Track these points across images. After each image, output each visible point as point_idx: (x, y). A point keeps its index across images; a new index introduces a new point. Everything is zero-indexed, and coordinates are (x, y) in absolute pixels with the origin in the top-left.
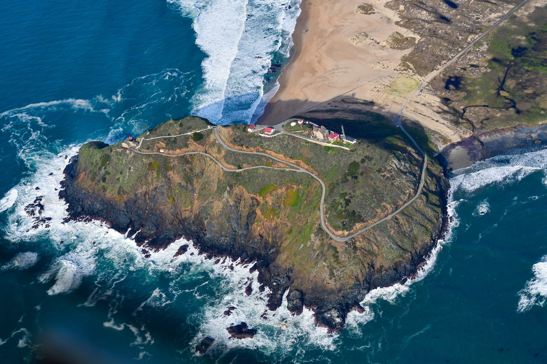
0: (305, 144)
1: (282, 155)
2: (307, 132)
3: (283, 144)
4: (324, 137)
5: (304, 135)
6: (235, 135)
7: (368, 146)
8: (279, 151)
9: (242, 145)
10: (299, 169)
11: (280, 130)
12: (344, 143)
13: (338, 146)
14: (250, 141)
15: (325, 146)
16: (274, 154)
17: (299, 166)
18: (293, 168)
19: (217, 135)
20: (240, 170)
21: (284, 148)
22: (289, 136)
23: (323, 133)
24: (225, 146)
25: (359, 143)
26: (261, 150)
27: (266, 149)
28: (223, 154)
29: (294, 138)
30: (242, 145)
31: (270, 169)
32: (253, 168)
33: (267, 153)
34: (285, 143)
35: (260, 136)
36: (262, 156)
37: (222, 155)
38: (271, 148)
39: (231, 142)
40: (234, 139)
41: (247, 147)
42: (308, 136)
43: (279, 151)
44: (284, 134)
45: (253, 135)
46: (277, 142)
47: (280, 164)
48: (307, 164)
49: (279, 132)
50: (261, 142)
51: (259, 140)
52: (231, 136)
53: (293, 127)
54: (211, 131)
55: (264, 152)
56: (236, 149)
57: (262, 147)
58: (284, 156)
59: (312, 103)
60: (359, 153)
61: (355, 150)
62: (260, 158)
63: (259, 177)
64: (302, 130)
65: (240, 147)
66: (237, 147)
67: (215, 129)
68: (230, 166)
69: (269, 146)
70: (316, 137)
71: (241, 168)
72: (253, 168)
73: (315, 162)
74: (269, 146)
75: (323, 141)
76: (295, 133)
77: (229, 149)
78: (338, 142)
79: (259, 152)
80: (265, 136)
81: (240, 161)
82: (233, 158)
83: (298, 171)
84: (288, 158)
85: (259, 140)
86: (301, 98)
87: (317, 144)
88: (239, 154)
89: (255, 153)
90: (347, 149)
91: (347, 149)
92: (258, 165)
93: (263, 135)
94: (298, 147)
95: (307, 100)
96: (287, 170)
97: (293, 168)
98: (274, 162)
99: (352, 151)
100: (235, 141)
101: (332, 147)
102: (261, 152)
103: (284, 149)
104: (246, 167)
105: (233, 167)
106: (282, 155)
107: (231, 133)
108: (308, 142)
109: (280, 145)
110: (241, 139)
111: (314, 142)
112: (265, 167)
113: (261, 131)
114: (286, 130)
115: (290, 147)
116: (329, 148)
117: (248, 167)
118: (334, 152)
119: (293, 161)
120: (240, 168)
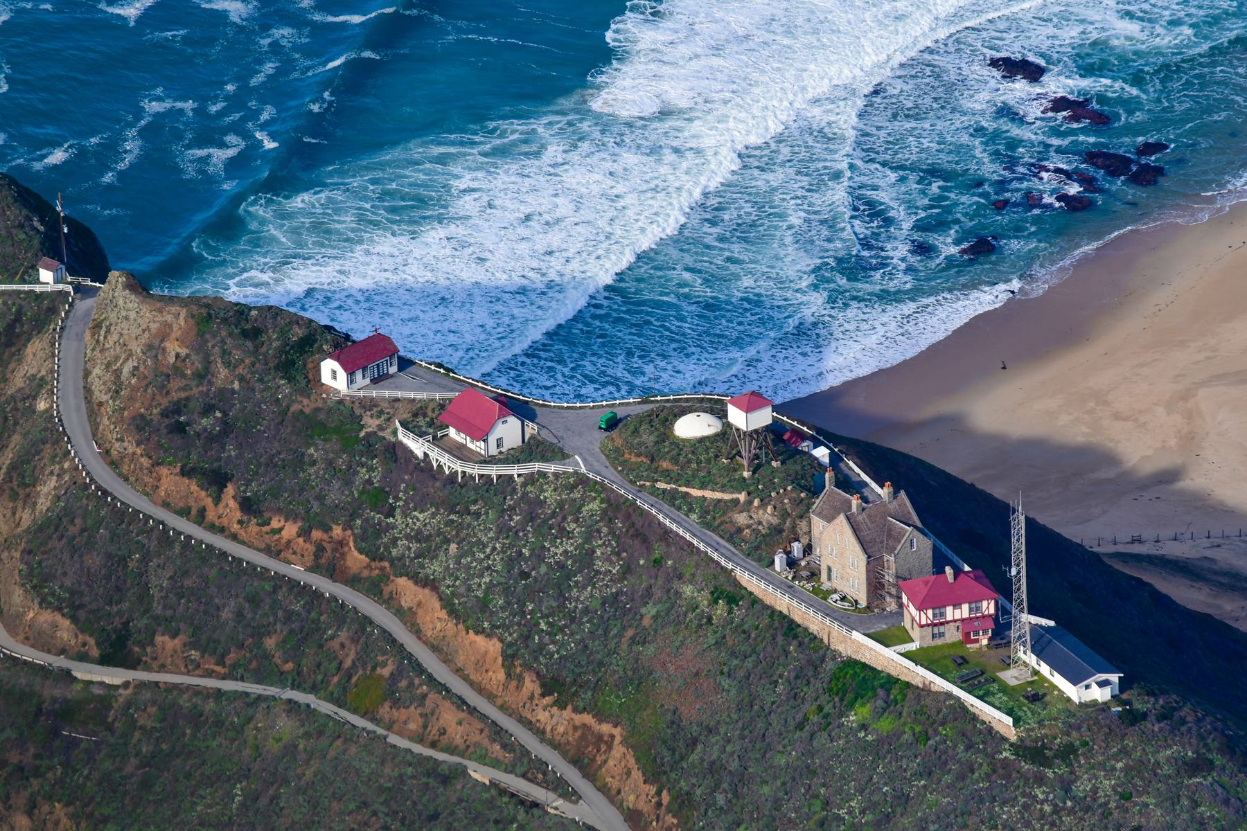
0: (704, 600)
1: (493, 647)
2: (767, 516)
3: (539, 555)
4: (875, 586)
5: (733, 536)
6: (200, 377)
7: (1198, 766)
8: (484, 605)
9: (217, 481)
10: (571, 795)
11: (569, 443)
12: (1011, 677)
13: (941, 684)
14: (300, 462)
15: (852, 663)
16: (435, 618)
17: (589, 770)
18: (535, 770)
19: (68, 349)
20: (113, 676)
21: (530, 594)
22: (615, 507)
23: (872, 544)
24: (85, 452)
25: (1132, 718)
26: (356, 559)
27: (400, 566)
28: (43, 504)
29: (642, 532)
30: (217, 481)
31: (345, 733)
32: (229, 685)
33: (390, 602)
34: (559, 550)
35: (396, 452)
36: (341, 611)
37: (26, 518)
38: (434, 568)
39: (141, 425)
40: (177, 408)
41: (247, 506)
42: (759, 550)
43: (484, 605)
44: (582, 480)
45: (343, 419)
46: (503, 530)
47: (449, 717)
48: (654, 774)
49: (559, 454)
50: (379, 498)
51: (372, 472)
52: (162, 378)
53: (679, 444)
54: (50, 305)
55: (375, 588)
56: (159, 497)
57: (371, 541)
58: (509, 658)
59: (1201, 505)
60: (1082, 787)
61: (1067, 753)
62: (310, 619)
63: (245, 775)
64: (742, 484)
65: (195, 491)
66: (170, 480)
67: (83, 305)
68: (46, 617)
69: (429, 544)
70: (814, 575)
71: (133, 664)
72: (229, 685)
73: (714, 769)
74: (429, 544)
75: (852, 616)
76: (671, 498)
77: (105, 477)
78: (963, 661)
79: (334, 571)
80: (439, 457)
81: (144, 596)
82: (94, 560)
83: (557, 805)
84: (531, 685)
85: (372, 472)
86: (1140, 450)
87: (790, 628)
88: (166, 537)
89: (297, 571)
90: (1001, 721)
91: (1001, 721)
92: (280, 678)
93: (417, 447)
94: (650, 611)
95: (1168, 477)
96: (480, 774)
97: (535, 770)
98: (406, 682)
99: (1032, 751)
100: (180, 429)
101: (891, 682)
102: (353, 581)
103: (522, 606)
104: (173, 671)
105: (65, 630)
106: (493, 647)
107: (173, 348)
108: (733, 595)
109: (510, 563)
110: (227, 427)
111: (782, 602)
112: (326, 707)
113: (419, 410)
114: (615, 457)
115: (583, 597)
116: (862, 681)
117: (192, 667)
118: (885, 725)
119: (558, 720)
120: (116, 652)
